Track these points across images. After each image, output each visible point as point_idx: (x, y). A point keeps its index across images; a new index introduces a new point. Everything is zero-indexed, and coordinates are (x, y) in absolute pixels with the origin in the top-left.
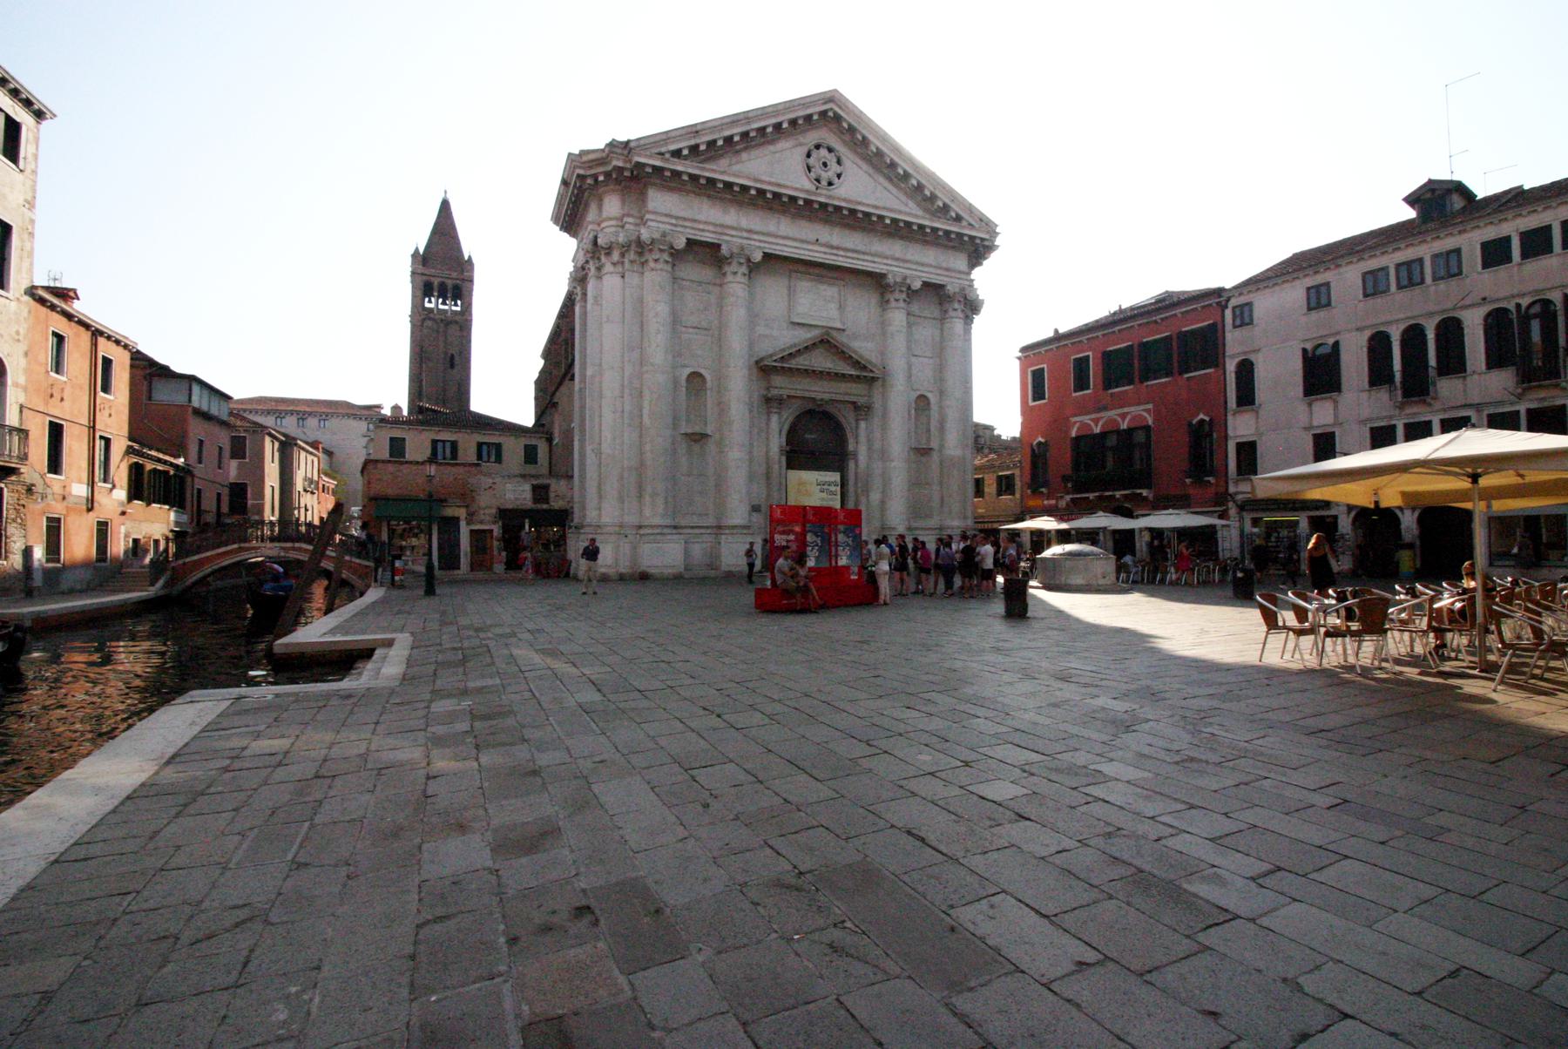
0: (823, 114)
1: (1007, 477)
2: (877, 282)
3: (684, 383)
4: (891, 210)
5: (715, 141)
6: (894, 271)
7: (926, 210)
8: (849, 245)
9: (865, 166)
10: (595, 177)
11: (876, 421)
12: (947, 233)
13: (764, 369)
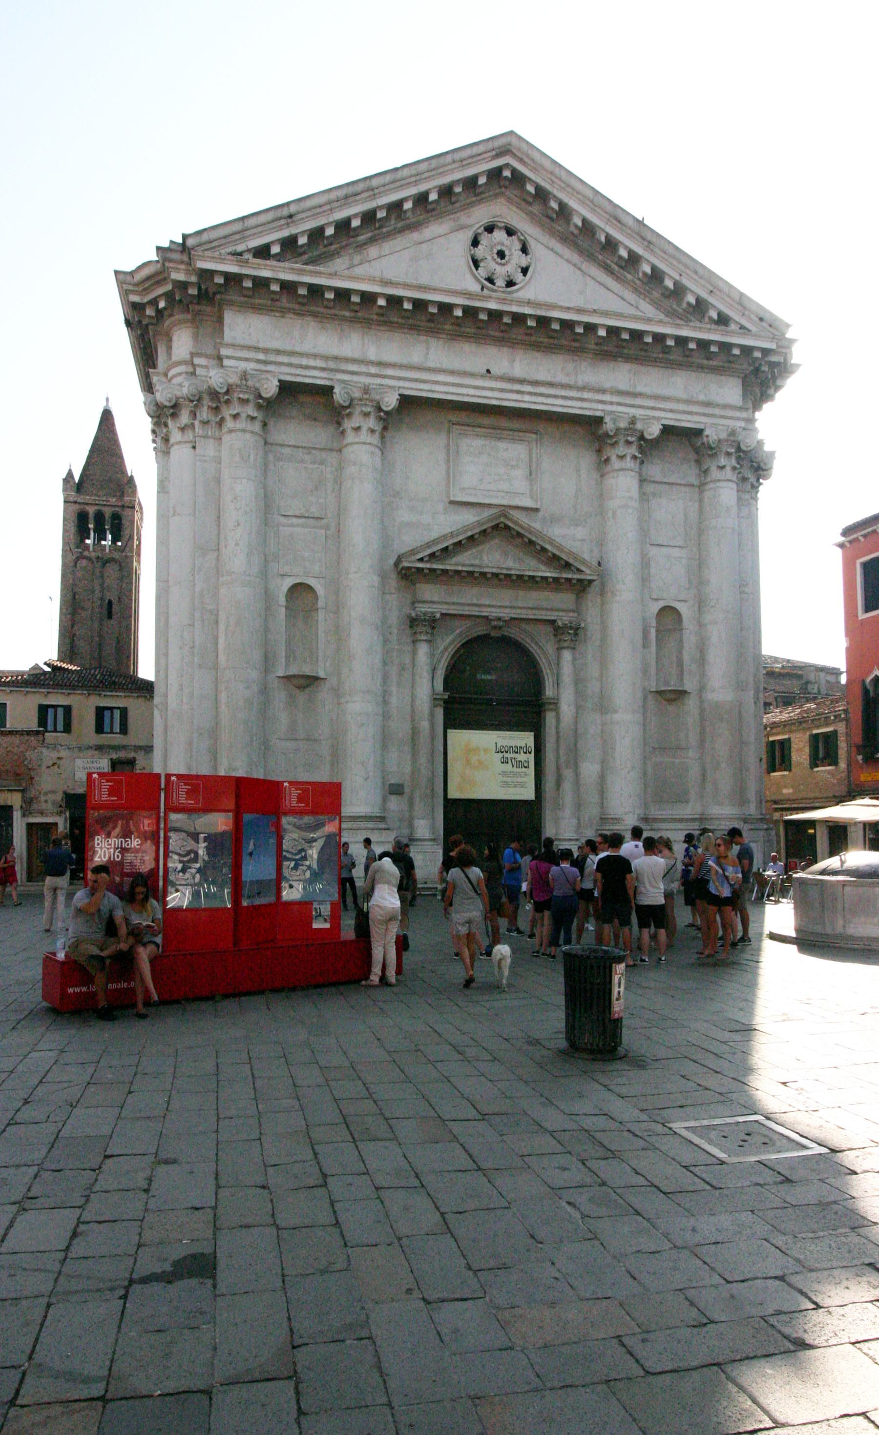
0: (495, 174)
1: (826, 736)
2: (589, 430)
3: (282, 600)
4: (606, 314)
5: (321, 230)
6: (615, 412)
7: (672, 314)
8: (542, 375)
9: (567, 252)
11: (590, 649)
12: (703, 345)
13: (408, 574)
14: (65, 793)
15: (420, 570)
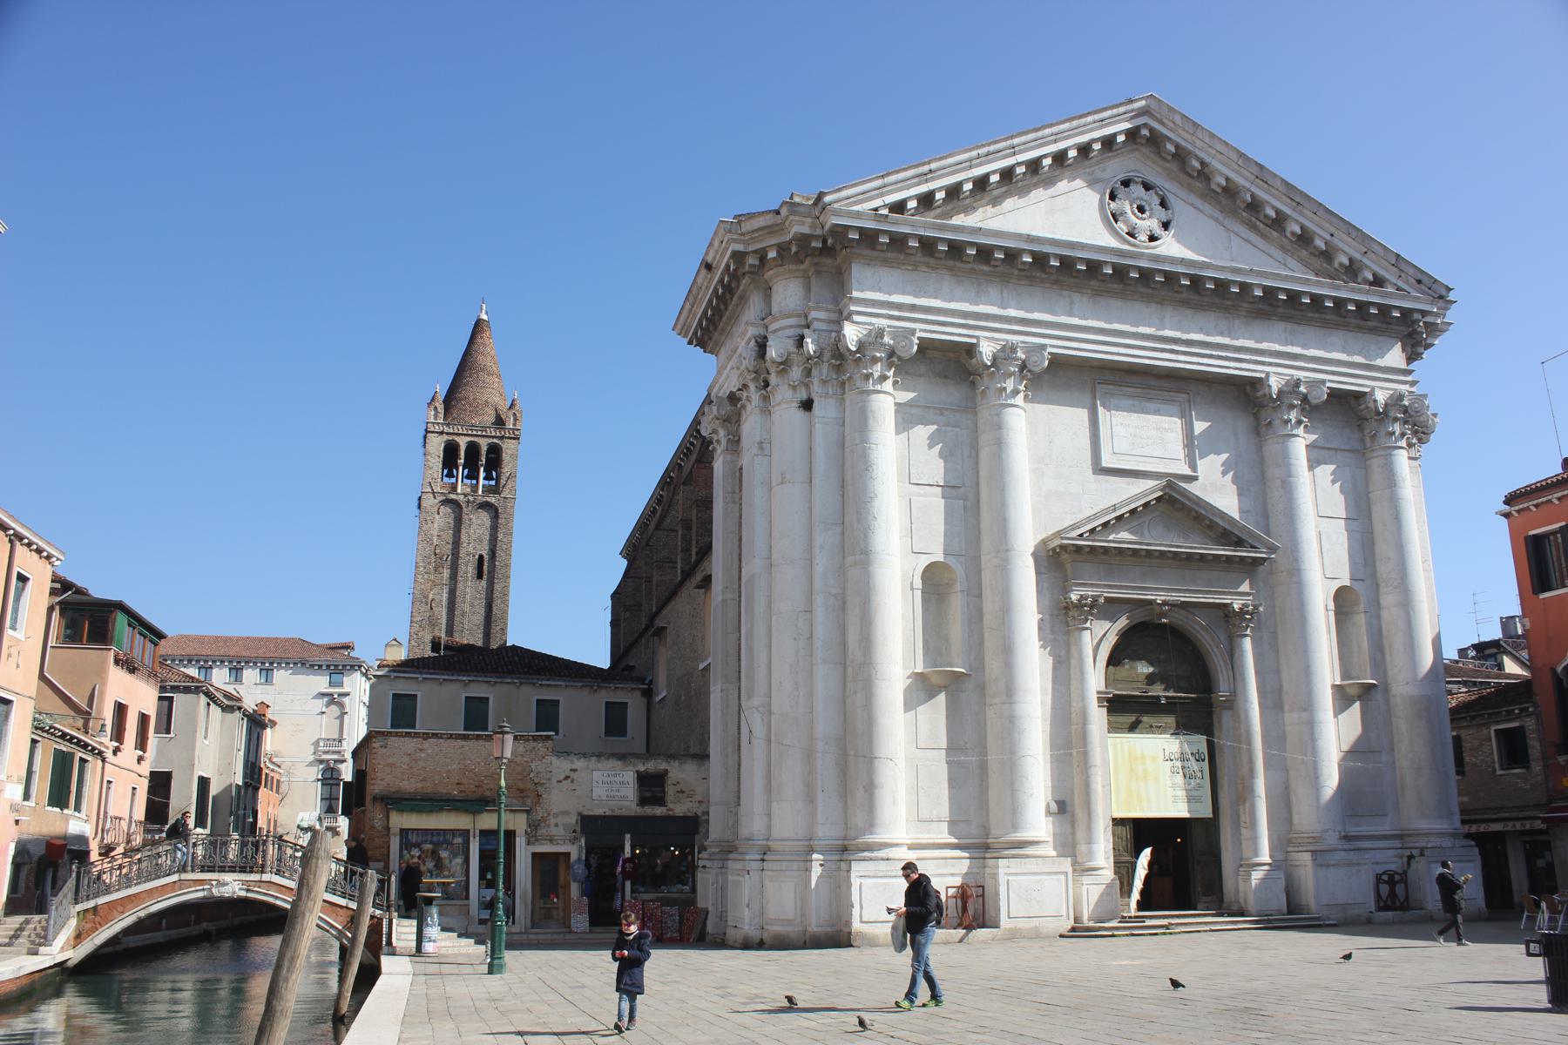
2: (1244, 398)
10: (762, 255)
12: (1362, 306)
14: (580, 814)
15: (1078, 549)
